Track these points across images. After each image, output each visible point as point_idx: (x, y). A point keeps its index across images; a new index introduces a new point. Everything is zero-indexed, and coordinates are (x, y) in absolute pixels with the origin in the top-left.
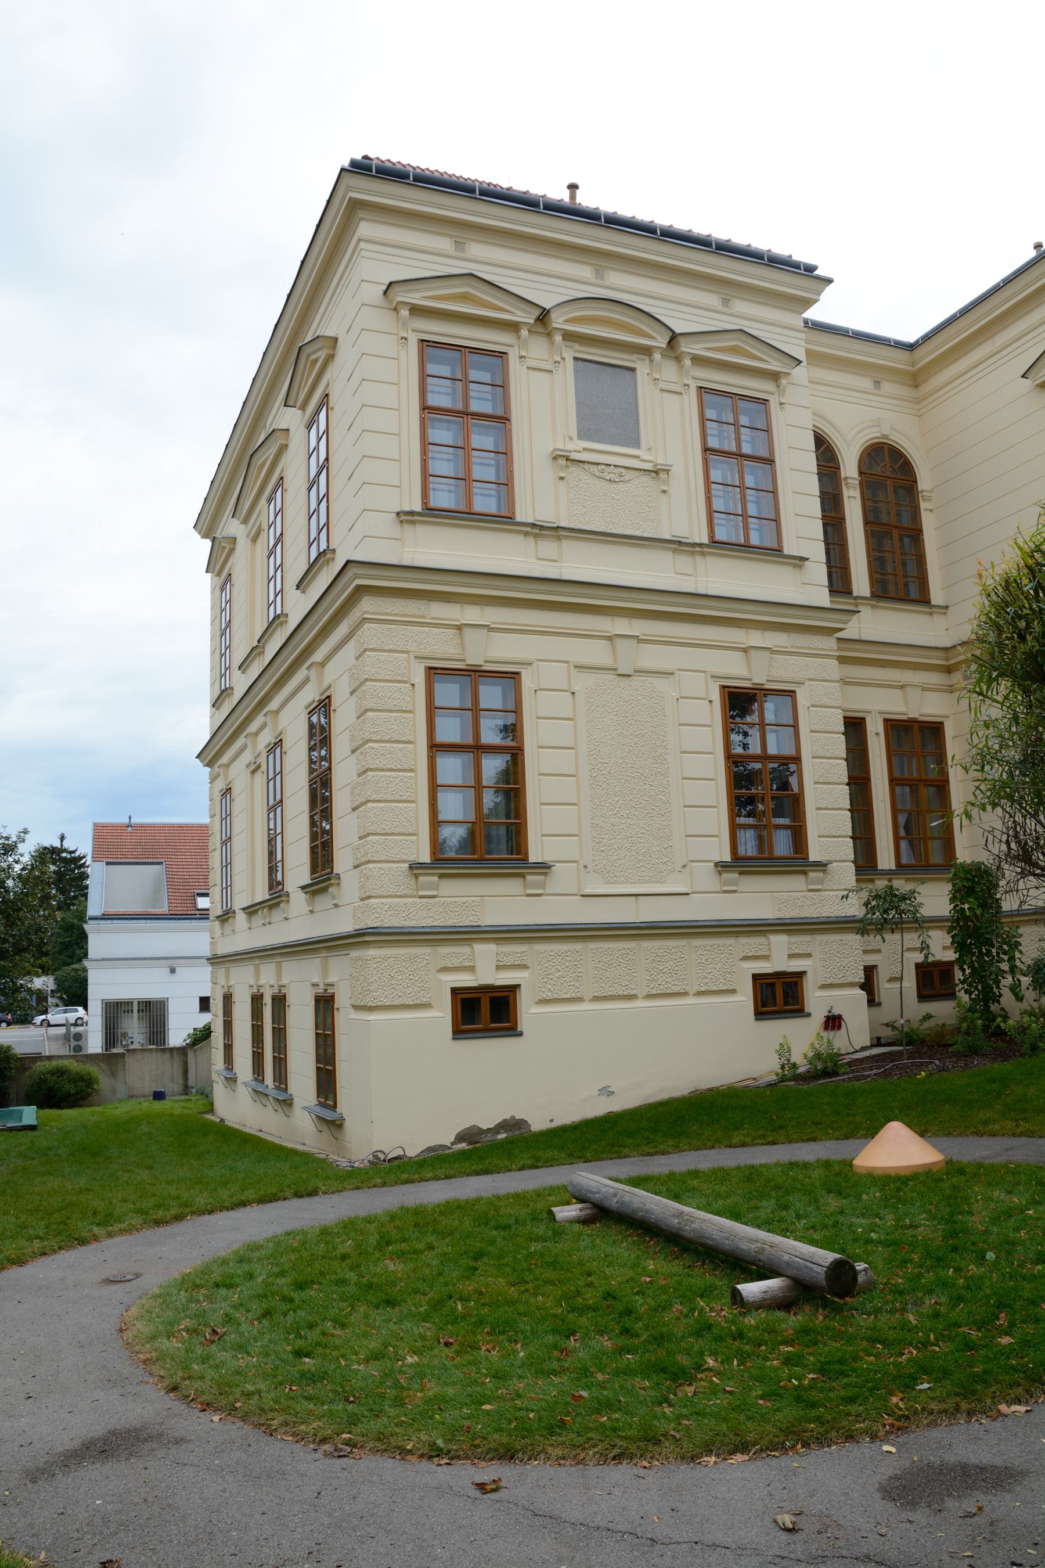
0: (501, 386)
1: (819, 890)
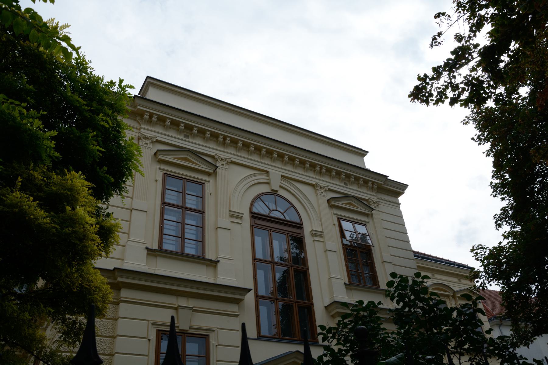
0: (202, 197)
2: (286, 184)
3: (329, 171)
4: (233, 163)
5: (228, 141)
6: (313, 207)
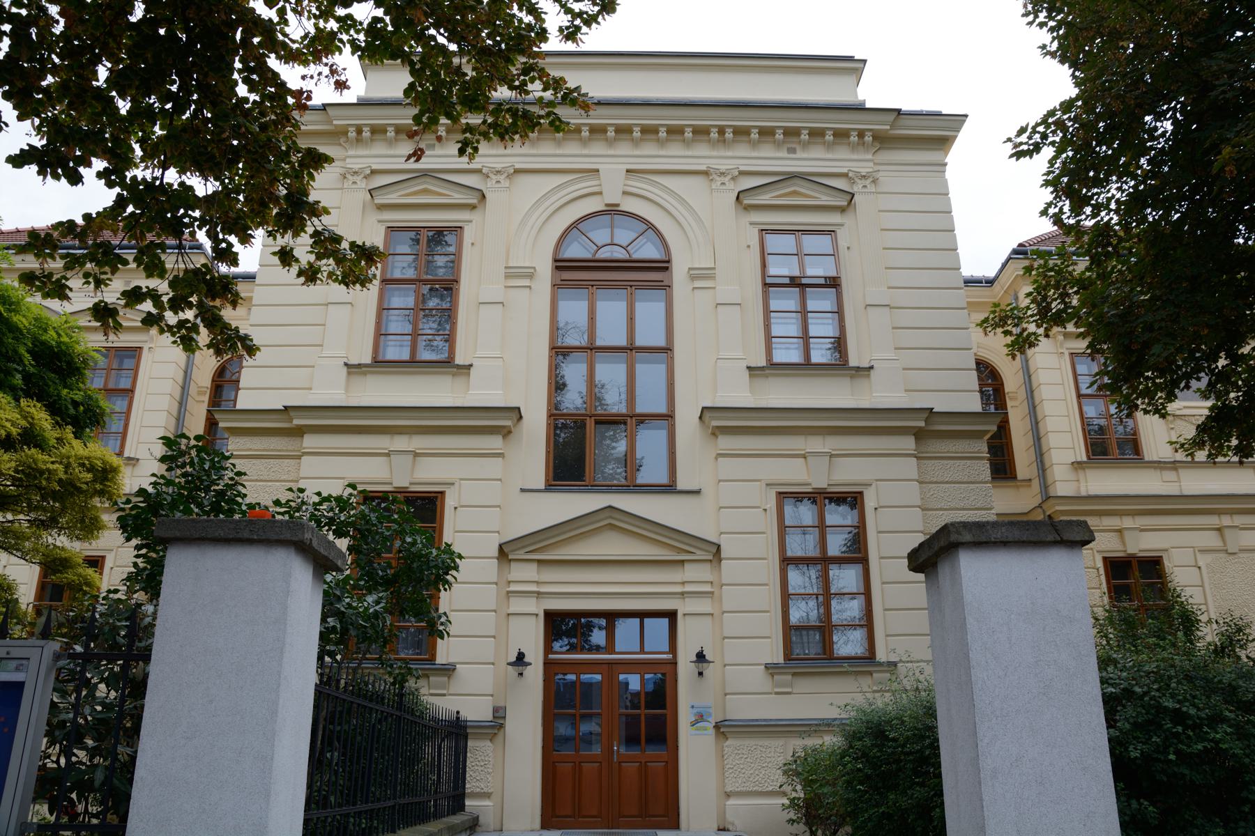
2: (637, 185)
3: (741, 132)
4: (518, 171)
5: (729, 135)
6: (699, 220)
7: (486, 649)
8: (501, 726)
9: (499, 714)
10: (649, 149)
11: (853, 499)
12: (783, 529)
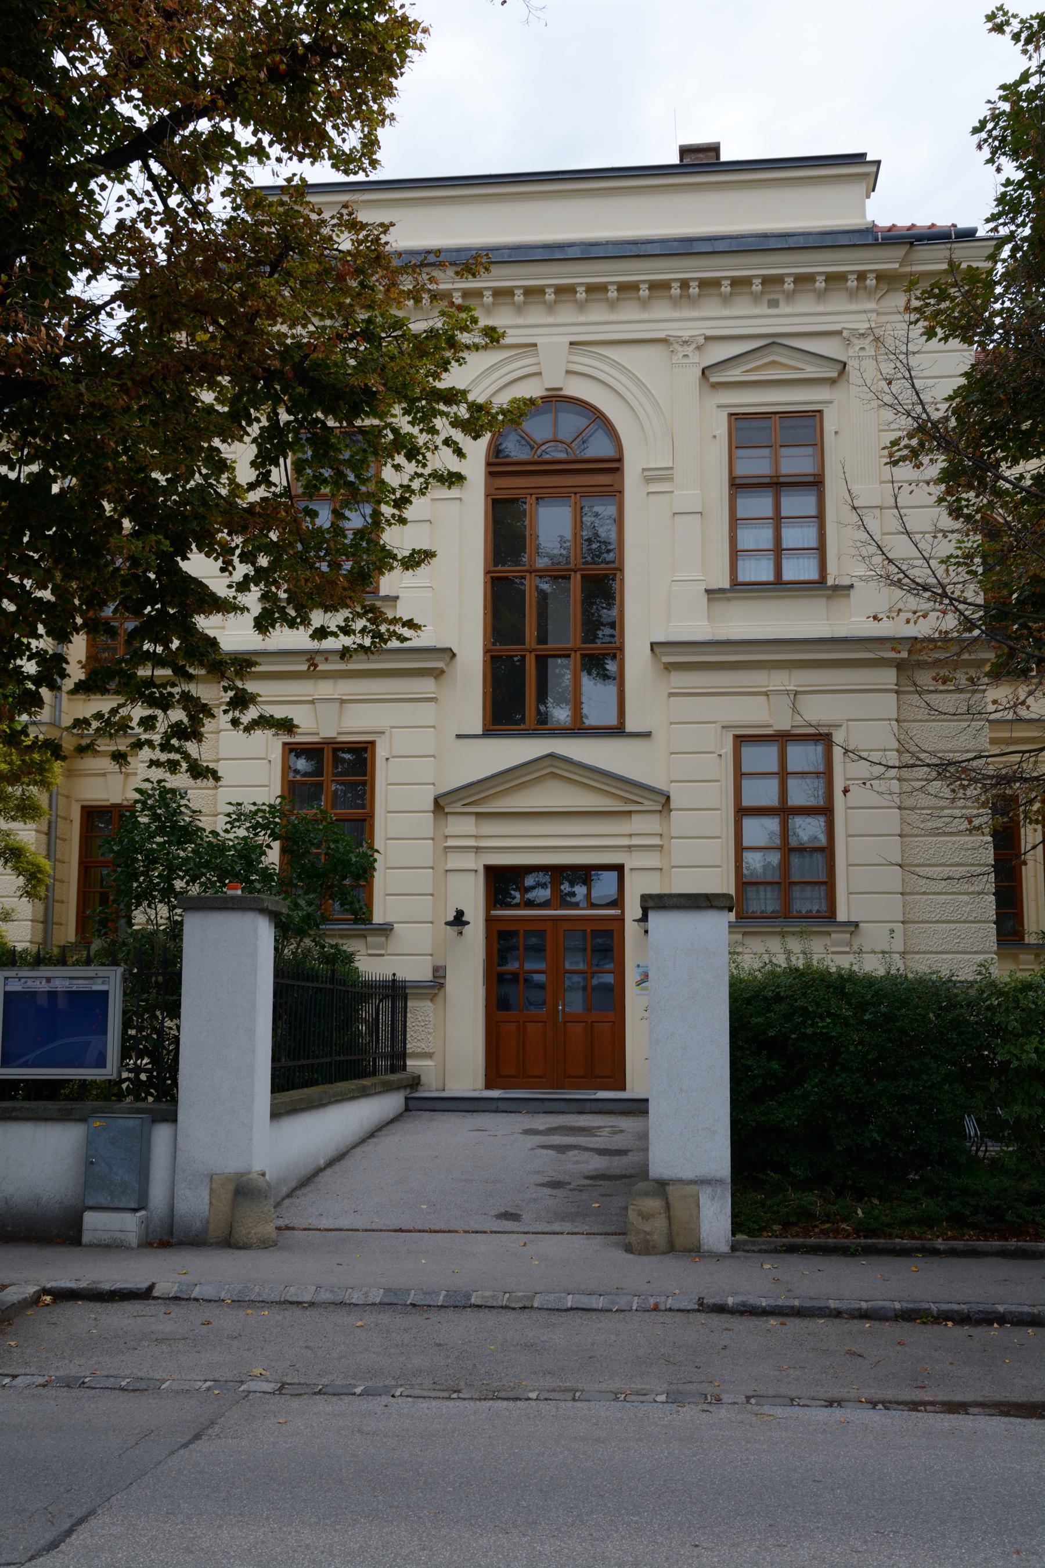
1: (382, 955)
2: (583, 362)
5: (694, 290)
7: (424, 908)
8: (442, 986)
9: (439, 975)
10: (598, 313)
11: (823, 739)
12: (739, 775)
